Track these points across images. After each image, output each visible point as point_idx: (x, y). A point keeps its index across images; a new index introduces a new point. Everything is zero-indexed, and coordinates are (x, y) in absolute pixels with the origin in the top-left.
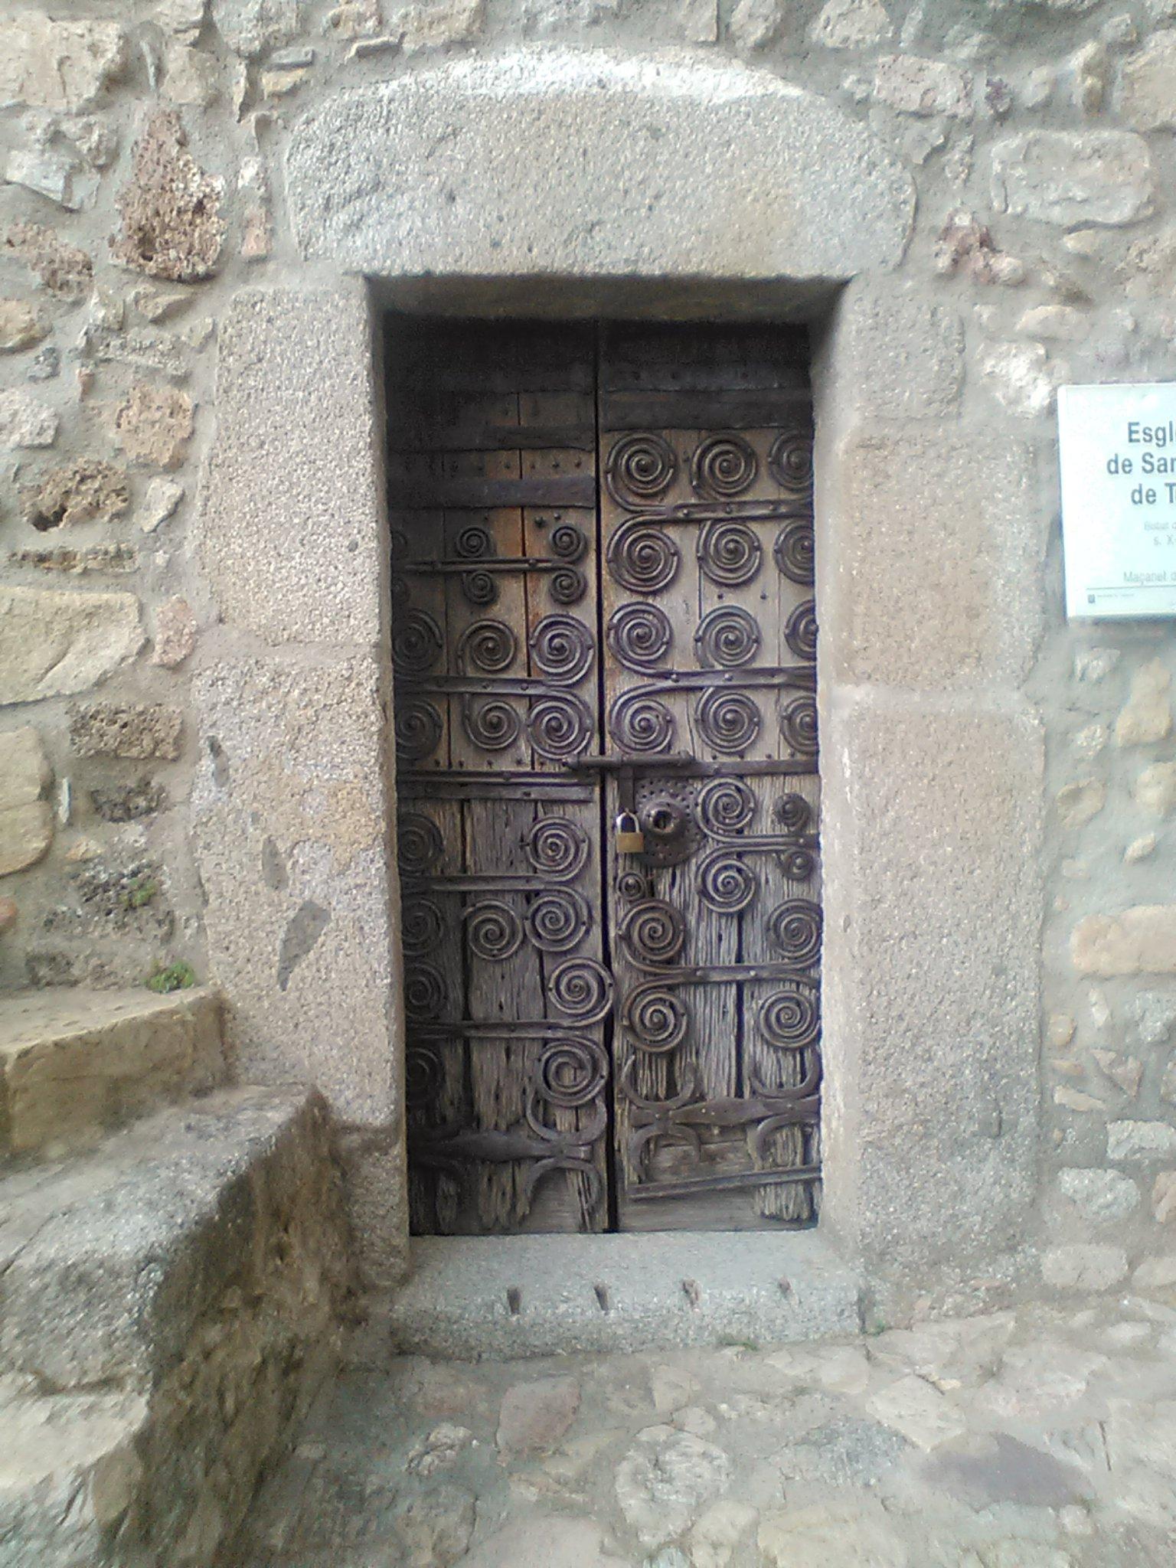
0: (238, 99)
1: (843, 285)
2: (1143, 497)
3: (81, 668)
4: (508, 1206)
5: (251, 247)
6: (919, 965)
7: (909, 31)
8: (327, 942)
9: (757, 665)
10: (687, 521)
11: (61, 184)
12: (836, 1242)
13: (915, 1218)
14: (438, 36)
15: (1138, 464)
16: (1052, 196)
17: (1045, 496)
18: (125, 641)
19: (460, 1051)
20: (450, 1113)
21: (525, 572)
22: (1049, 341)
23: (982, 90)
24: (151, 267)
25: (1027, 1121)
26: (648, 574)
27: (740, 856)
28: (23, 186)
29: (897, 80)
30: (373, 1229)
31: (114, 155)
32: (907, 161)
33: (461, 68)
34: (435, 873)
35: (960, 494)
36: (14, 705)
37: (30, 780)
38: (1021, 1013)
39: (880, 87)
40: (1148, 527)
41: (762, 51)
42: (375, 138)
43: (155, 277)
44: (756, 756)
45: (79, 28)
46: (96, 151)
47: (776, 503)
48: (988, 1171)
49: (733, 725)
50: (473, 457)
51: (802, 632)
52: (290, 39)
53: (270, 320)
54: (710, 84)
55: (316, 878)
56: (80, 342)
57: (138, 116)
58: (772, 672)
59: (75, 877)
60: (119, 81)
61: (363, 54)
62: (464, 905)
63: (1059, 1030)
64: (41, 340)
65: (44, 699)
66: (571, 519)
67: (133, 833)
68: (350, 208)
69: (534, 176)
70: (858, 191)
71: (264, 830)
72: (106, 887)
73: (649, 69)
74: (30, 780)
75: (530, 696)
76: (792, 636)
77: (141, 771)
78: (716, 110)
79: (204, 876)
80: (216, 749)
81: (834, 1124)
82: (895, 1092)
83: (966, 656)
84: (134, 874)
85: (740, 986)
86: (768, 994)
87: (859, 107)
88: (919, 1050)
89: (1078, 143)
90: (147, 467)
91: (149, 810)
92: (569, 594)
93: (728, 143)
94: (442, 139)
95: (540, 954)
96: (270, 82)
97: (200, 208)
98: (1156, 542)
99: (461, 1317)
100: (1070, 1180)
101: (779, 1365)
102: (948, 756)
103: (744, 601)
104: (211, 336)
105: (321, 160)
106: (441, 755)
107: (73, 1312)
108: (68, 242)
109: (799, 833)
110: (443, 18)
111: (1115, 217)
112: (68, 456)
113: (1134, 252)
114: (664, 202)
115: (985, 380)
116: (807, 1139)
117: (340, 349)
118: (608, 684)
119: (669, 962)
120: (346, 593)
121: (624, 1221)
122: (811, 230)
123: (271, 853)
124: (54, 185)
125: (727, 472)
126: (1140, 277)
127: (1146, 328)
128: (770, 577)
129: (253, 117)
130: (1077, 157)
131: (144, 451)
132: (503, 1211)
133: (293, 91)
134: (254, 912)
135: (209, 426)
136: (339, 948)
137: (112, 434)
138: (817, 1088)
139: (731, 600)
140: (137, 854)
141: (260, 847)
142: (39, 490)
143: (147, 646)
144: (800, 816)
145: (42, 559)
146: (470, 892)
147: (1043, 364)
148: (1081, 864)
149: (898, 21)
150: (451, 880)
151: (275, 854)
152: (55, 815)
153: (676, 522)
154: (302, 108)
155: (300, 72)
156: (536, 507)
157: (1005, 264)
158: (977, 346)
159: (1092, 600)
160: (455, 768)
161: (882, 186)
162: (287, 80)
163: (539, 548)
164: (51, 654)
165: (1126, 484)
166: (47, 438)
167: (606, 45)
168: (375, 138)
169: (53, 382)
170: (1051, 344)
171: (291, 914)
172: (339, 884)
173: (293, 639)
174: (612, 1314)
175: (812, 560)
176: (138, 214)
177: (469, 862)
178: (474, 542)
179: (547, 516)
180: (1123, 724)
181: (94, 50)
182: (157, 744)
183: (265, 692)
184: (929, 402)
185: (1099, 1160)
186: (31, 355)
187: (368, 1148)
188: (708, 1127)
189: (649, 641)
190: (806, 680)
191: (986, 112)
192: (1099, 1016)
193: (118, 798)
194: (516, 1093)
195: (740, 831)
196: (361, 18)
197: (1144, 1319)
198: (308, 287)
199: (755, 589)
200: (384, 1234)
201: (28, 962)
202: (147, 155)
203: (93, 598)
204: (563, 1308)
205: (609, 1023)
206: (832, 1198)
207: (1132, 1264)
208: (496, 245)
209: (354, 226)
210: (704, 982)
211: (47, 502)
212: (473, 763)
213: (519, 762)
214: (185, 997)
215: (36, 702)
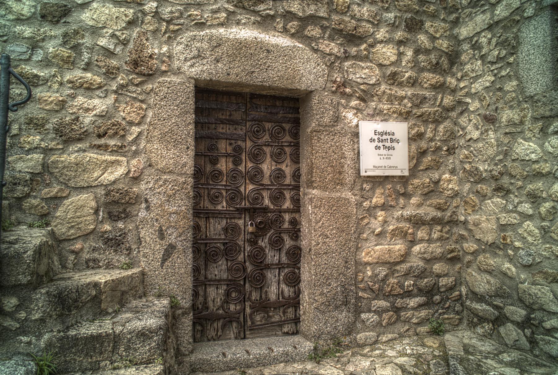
1: (311, 92)
2: (377, 148)
3: (108, 177)
4: (215, 333)
6: (328, 261)
7: (327, 35)
9: (285, 183)
10: (268, 145)
14: (215, 22)
15: (377, 140)
16: (358, 76)
17: (356, 146)
18: (122, 170)
20: (200, 306)
21: (226, 156)
22: (357, 109)
23: (342, 50)
26: (256, 157)
28: (102, 47)
30: (184, 337)
31: (128, 41)
33: (222, 30)
37: (92, 208)
38: (351, 273)
39: (322, 47)
40: (378, 155)
41: (293, 36)
42: (198, 45)
43: (137, 74)
48: (344, 315)
49: (277, 198)
51: (296, 175)
52: (178, 18)
53: (168, 88)
54: (282, 41)
58: (289, 185)
59: (102, 236)
60: (131, 23)
61: (196, 24)
62: (206, 247)
64: (104, 87)
65: (98, 186)
66: (239, 143)
67: (121, 225)
70: (315, 71)
71: (159, 224)
72: (112, 239)
73: (267, 36)
78: (283, 48)
79: (141, 236)
80: (146, 201)
83: (339, 183)
84: (120, 236)
87: (316, 51)
89: (363, 65)
91: (125, 218)
94: (216, 47)
97: (151, 57)
98: (380, 159)
99: (210, 360)
100: (363, 316)
101: (296, 366)
102: (335, 208)
105: (184, 48)
107: (140, 343)
110: (218, 18)
111: (371, 82)
113: (375, 91)
117: (187, 96)
119: (261, 262)
120: (185, 160)
122: (304, 78)
124: (112, 47)
132: (213, 334)
133: (178, 30)
134: (155, 247)
136: (178, 257)
138: (299, 296)
141: (157, 228)
142: (100, 127)
143: (129, 171)
144: (295, 223)
146: (208, 243)
147: (355, 114)
149: (324, 33)
150: (203, 240)
151: (162, 230)
153: (265, 145)
156: (230, 139)
157: (348, 90)
159: (366, 172)
160: (205, 208)
162: (177, 27)
163: (230, 150)
168: (198, 45)
170: (358, 110)
171: (165, 247)
176: (134, 56)
180: (374, 200)
181: (126, 16)
182: (130, 198)
183: (161, 186)
184: (331, 122)
185: (370, 311)
187: (183, 314)
188: (270, 308)
189: (255, 176)
190: (297, 188)
193: (116, 214)
195: (280, 227)
196: (197, 15)
197: (381, 349)
198: (179, 80)
200: (187, 338)
202: (137, 42)
203: (114, 158)
208: (228, 74)
209: (192, 66)
212: (211, 207)
215: (95, 186)
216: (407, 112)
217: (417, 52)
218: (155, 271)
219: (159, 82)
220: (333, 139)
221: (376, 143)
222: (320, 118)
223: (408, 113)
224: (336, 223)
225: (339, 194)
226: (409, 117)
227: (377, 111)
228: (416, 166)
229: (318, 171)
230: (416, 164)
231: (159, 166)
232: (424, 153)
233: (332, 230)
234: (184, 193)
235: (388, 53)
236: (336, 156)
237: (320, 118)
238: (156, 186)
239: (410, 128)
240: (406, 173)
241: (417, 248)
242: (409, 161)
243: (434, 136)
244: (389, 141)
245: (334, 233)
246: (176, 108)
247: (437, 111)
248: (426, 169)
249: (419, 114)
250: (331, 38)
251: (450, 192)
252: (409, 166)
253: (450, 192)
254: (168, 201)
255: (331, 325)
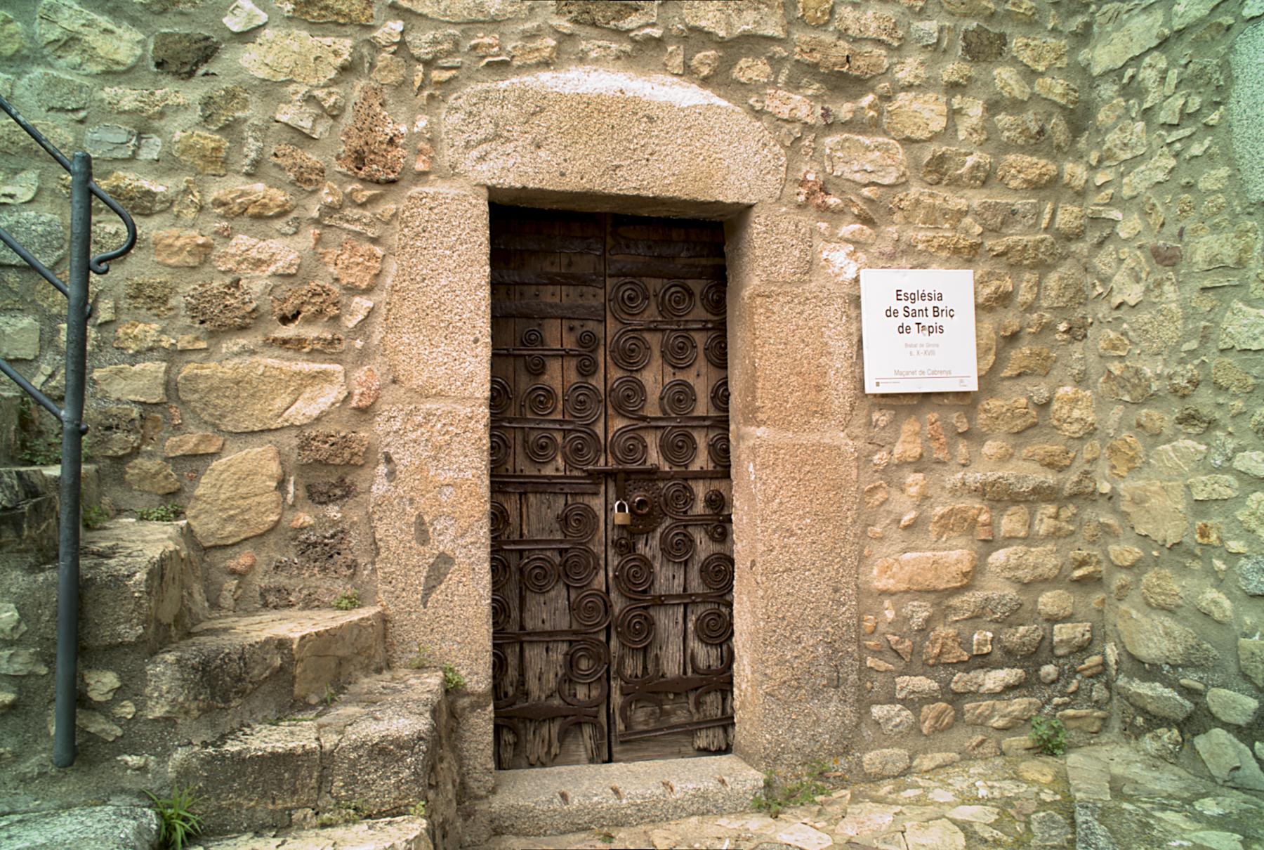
0: (418, 84)
1: (751, 206)
2: (904, 329)
3: (307, 408)
5: (420, 166)
7: (782, 78)
8: (453, 577)
9: (695, 414)
10: (656, 330)
11: (310, 124)
12: (747, 758)
13: (793, 738)
14: (532, 59)
15: (901, 312)
16: (856, 168)
18: (335, 393)
19: (517, 649)
20: (511, 691)
21: (562, 356)
23: (819, 111)
24: (362, 174)
25: (853, 677)
26: (629, 358)
27: (685, 526)
29: (777, 103)
32: (783, 146)
33: (545, 76)
34: (504, 538)
35: (811, 324)
36: (262, 431)
37: (271, 477)
41: (705, 82)
42: (495, 111)
43: (363, 180)
44: (695, 467)
45: (328, 41)
46: (334, 106)
47: (706, 322)
48: (832, 707)
49: (679, 447)
50: (534, 288)
51: (721, 396)
52: (449, 54)
55: (447, 538)
56: (316, 214)
57: (358, 88)
59: (295, 539)
61: (489, 64)
62: (521, 558)
63: (868, 625)
64: (291, 211)
65: (282, 428)
66: (591, 326)
67: (333, 512)
68: (480, 148)
69: (584, 138)
72: (315, 545)
73: (648, 86)
74: (271, 477)
75: (564, 430)
76: (714, 398)
77: (340, 472)
79: (378, 536)
80: (388, 459)
81: (744, 686)
82: (781, 662)
83: (816, 412)
84: (332, 537)
85: (686, 605)
86: (701, 609)
87: (758, 114)
88: (794, 637)
90: (352, 290)
91: (342, 497)
92: (586, 370)
93: (690, 128)
95: (568, 587)
96: (436, 75)
100: (877, 711)
102: (807, 468)
103: (690, 377)
104: (395, 215)
105: (464, 120)
106: (510, 466)
107: (376, 771)
108: (312, 157)
109: (718, 514)
110: (538, 50)
111: (886, 181)
112: (305, 281)
113: (897, 199)
114: (655, 157)
115: (824, 263)
116: (724, 700)
118: (610, 424)
119: (644, 592)
120: (471, 368)
121: (616, 756)
123: (420, 522)
124: (306, 124)
125: (678, 303)
126: (900, 213)
127: (904, 239)
128: (702, 364)
129: (426, 93)
130: (867, 148)
131: (352, 280)
133: (449, 81)
135: (392, 266)
137: (331, 269)
138: (730, 667)
139: (680, 376)
140: (334, 523)
141: (413, 519)
143: (350, 395)
144: (720, 505)
145: (285, 342)
148: (878, 529)
149: (777, 73)
151: (422, 523)
152: (285, 499)
153: (649, 330)
154: (455, 90)
155: (454, 72)
158: (819, 244)
159: (878, 384)
160: (518, 473)
161: (770, 156)
162: (446, 75)
163: (570, 343)
164: (288, 400)
165: (896, 322)
166: (293, 271)
167: (626, 69)
168: (495, 111)
169: (296, 237)
171: (431, 561)
172: (461, 542)
173: (438, 394)
174: (624, 801)
175: (726, 354)
176: (356, 143)
177: (525, 531)
178: (533, 337)
179: (576, 323)
180: (898, 449)
183: (420, 425)
184: (795, 273)
185: (892, 700)
186: (285, 220)
187: (473, 707)
189: (627, 399)
190: (722, 423)
191: (822, 122)
192: (890, 615)
194: (552, 676)
195: (685, 512)
196: (491, 46)
197: (919, 787)
199: (693, 371)
200: (483, 761)
201: (261, 594)
204: (595, 799)
205: (608, 629)
206: (742, 733)
207: (911, 758)
210: (662, 604)
211: (288, 308)
212: (530, 470)
213: (557, 470)
214: (367, 612)
215: (277, 429)
216: (971, 246)
217: (993, 107)
218: (410, 613)
219: (411, 197)
220: (801, 313)
221: (901, 319)
222: (771, 265)
223: (975, 248)
224: (811, 501)
225: (815, 437)
226: (977, 258)
227: (902, 246)
228: (993, 370)
229: (768, 385)
230: (994, 363)
231: (414, 381)
232: (1014, 338)
233: (802, 518)
234: (469, 439)
235: (925, 112)
236: (808, 351)
237: (771, 265)
238: (408, 426)
239: (980, 282)
240: (972, 385)
241: (998, 557)
242: (979, 359)
243: (1037, 297)
244: (930, 312)
245: (806, 525)
246: (448, 252)
247: (1043, 241)
248: (1019, 375)
249: (999, 249)
250: (793, 85)
251: (1075, 427)
252: (979, 370)
253: (1075, 427)
254: (435, 458)
255: (804, 733)
